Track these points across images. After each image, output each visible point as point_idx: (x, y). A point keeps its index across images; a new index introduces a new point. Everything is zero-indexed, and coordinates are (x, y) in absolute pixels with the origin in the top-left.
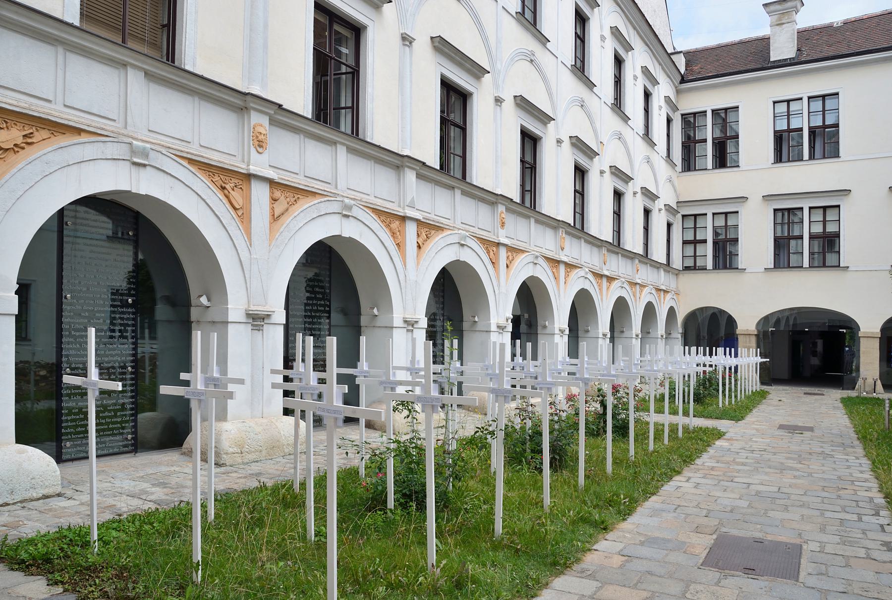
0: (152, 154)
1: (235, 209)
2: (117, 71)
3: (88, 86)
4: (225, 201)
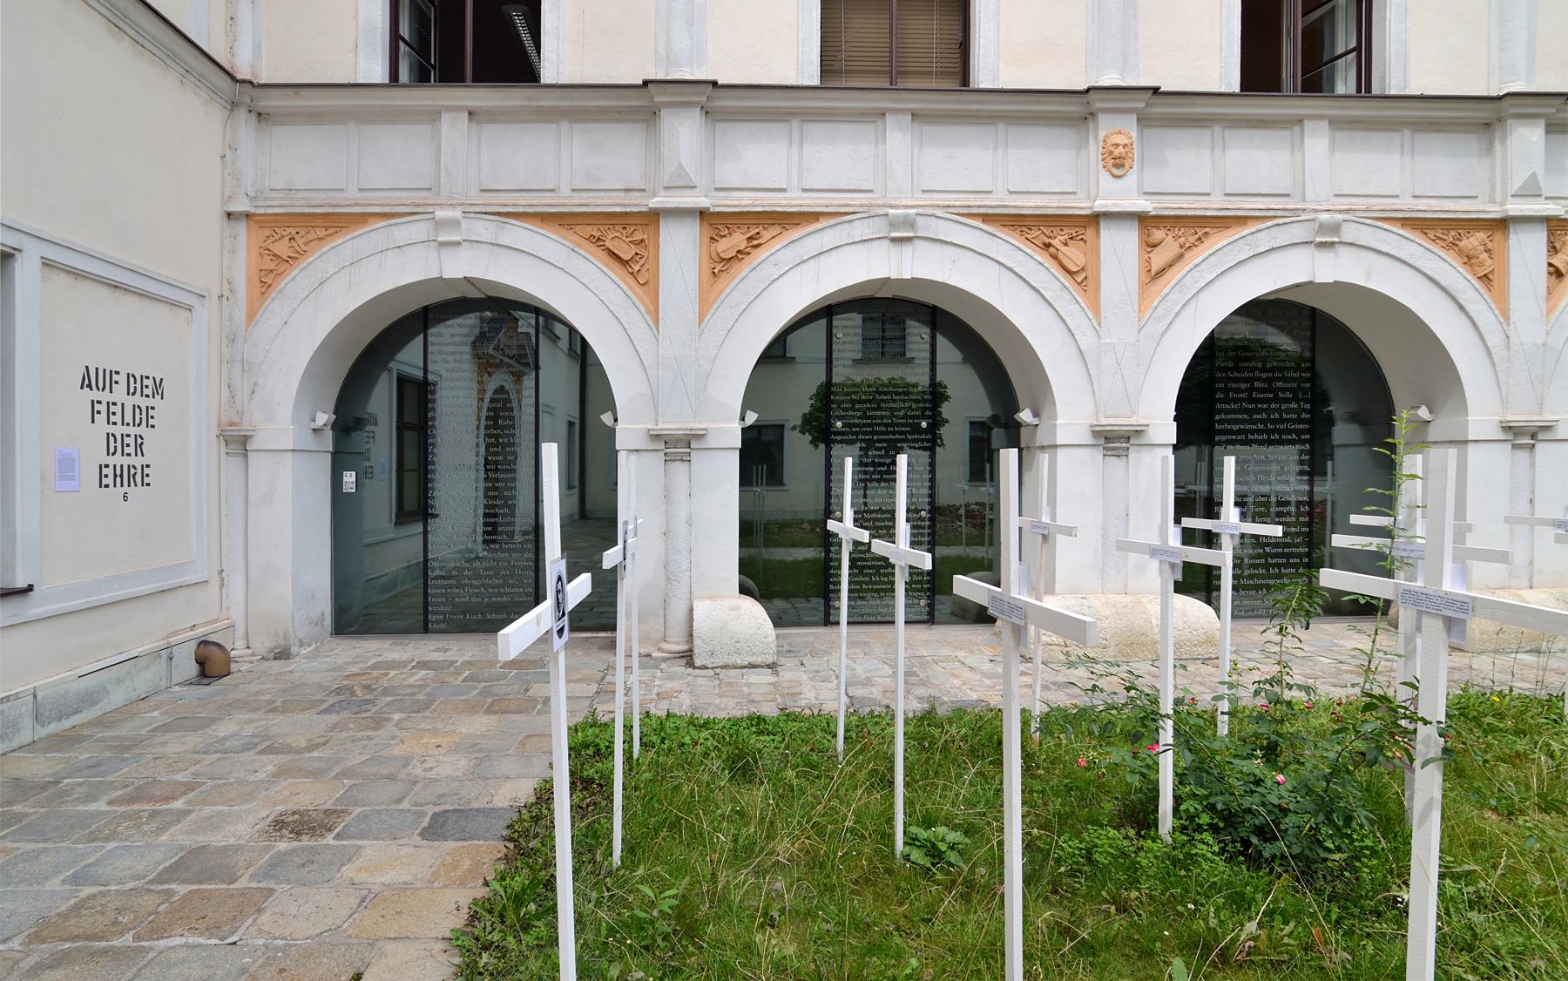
0: (920, 221)
1: (1071, 273)
2: (873, 126)
4: (1049, 263)
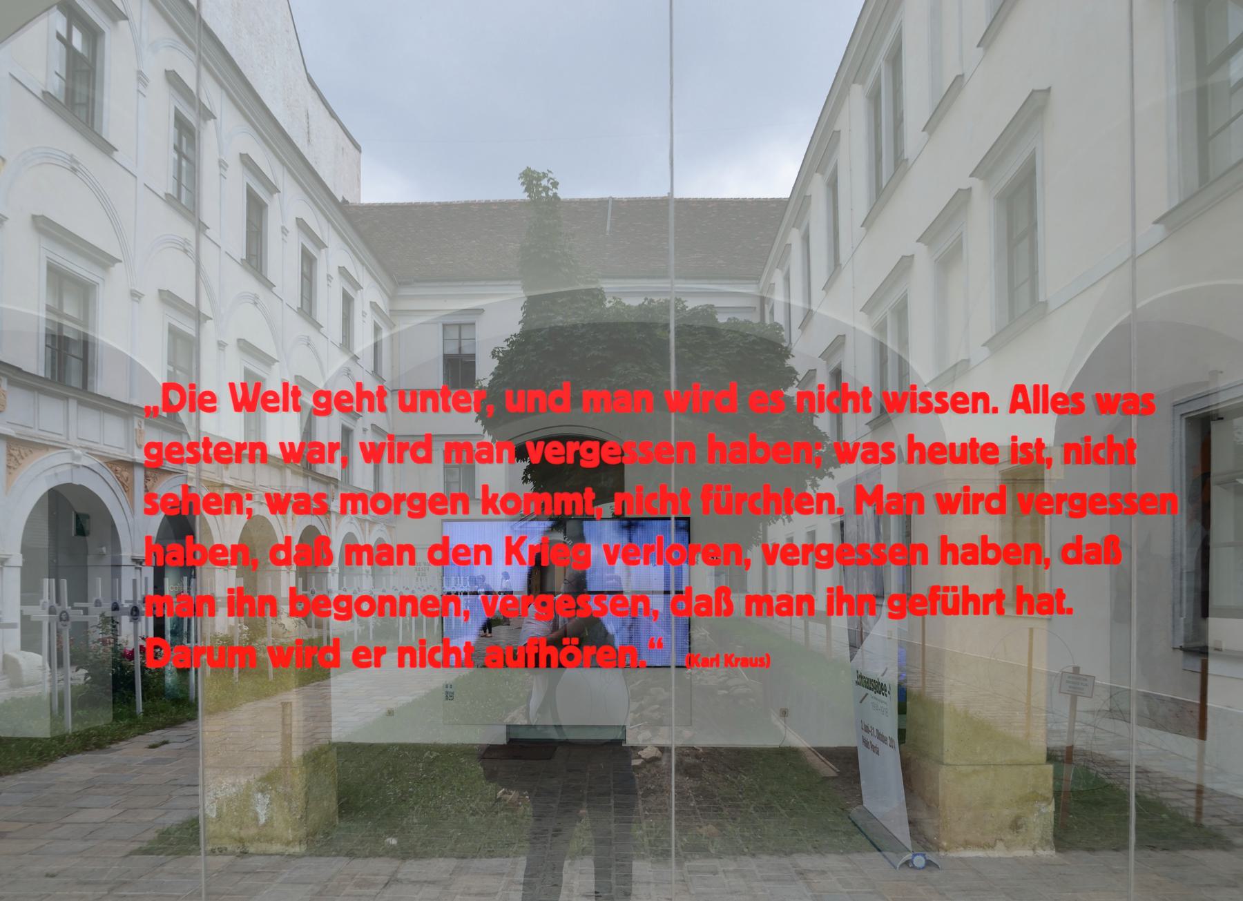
3: (47, 416)
